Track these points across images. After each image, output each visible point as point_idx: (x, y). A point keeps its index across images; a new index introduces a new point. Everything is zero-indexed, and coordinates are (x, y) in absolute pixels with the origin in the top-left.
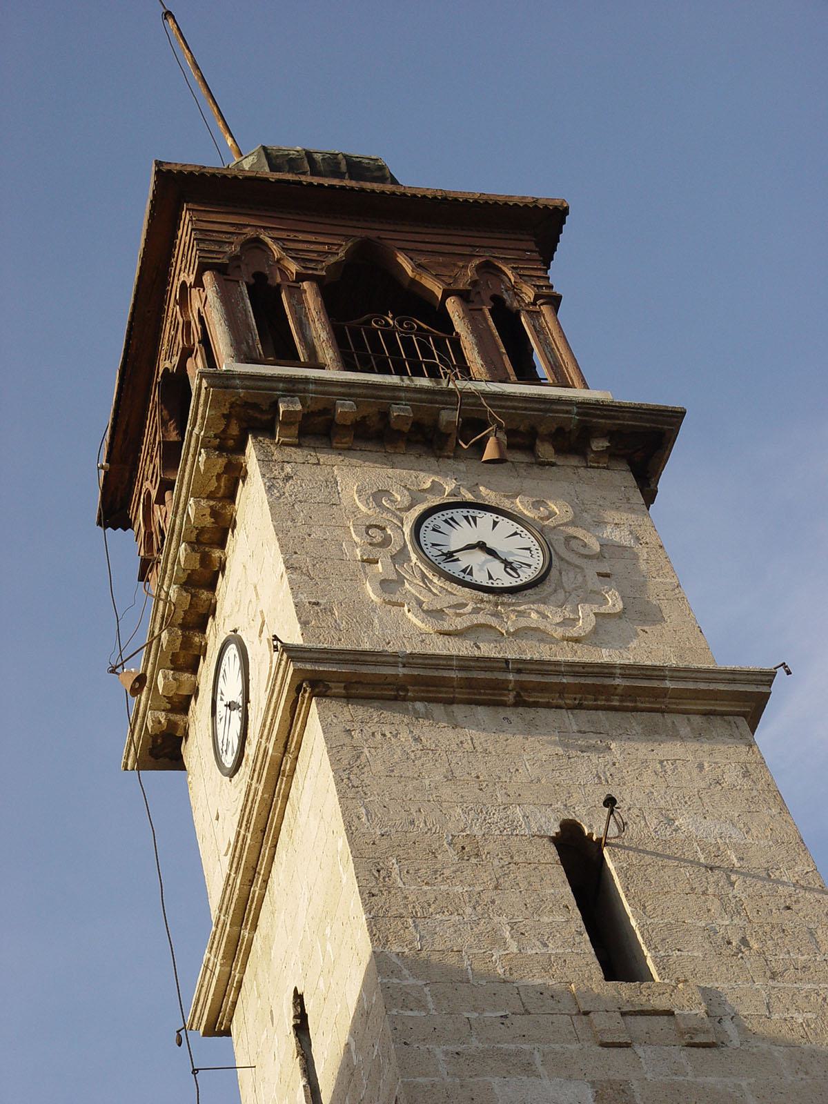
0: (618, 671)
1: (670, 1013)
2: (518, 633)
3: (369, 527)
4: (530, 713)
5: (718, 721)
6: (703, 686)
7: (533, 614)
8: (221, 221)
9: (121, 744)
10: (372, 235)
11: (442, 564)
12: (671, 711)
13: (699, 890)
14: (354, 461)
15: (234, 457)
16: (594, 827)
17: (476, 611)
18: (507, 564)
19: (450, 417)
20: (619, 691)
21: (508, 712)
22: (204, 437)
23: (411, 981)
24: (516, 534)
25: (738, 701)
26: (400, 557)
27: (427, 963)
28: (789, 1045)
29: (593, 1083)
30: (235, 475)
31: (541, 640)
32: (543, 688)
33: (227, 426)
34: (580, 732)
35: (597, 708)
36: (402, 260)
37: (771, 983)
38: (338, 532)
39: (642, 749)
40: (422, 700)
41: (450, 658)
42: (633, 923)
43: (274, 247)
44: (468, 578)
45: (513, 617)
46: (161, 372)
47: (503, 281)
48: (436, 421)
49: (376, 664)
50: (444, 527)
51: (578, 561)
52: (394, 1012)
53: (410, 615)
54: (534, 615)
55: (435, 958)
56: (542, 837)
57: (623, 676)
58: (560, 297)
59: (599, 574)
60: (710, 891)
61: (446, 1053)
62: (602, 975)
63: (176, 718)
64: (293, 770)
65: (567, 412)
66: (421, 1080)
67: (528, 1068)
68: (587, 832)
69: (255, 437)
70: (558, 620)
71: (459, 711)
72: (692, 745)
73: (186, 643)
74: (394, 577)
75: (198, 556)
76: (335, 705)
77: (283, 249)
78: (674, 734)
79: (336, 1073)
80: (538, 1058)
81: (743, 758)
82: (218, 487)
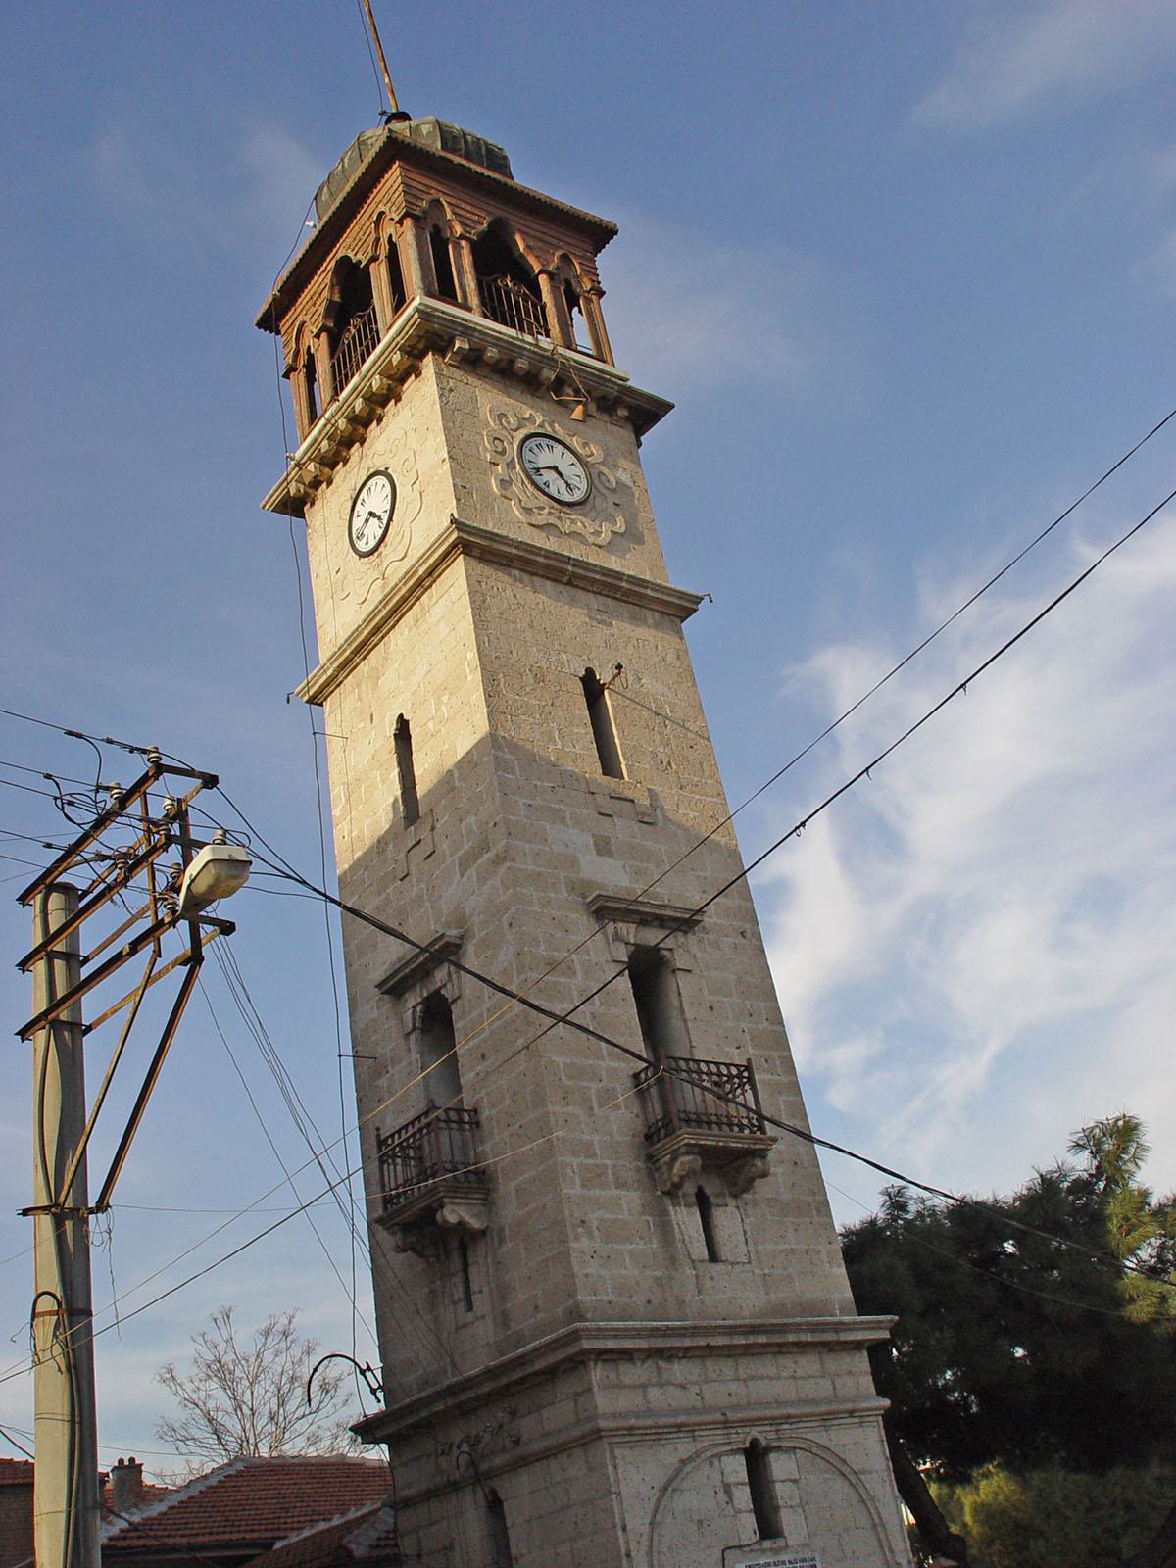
0: (626, 578)
1: (632, 801)
2: (573, 535)
3: (495, 439)
4: (573, 591)
5: (667, 618)
6: (666, 598)
7: (580, 523)
8: (420, 180)
9: (273, 494)
10: (504, 214)
11: (532, 474)
12: (646, 607)
13: (651, 727)
14: (488, 387)
15: (417, 362)
16: (603, 676)
17: (550, 514)
18: (568, 485)
19: (549, 375)
20: (623, 590)
21: (562, 588)
22: (402, 344)
23: (508, 756)
24: (573, 464)
25: (678, 608)
26: (510, 465)
27: (517, 746)
28: (686, 830)
29: (593, 835)
30: (414, 371)
31: (582, 542)
32: (585, 578)
33: (418, 342)
34: (598, 610)
35: (607, 596)
36: (518, 238)
37: (681, 792)
38: (478, 437)
39: (628, 628)
40: (519, 570)
41: (540, 549)
42: (617, 741)
43: (448, 210)
44: (546, 490)
45: (568, 522)
46: (338, 257)
47: (572, 270)
48: (539, 372)
49: (501, 543)
50: (536, 449)
51: (604, 491)
52: (499, 773)
53: (514, 508)
54: (579, 524)
55: (521, 743)
56: (576, 676)
57: (627, 581)
58: (604, 293)
59: (615, 504)
60: (656, 729)
61: (525, 804)
62: (601, 772)
63: (310, 491)
64: (430, 586)
65: (612, 388)
66: (511, 817)
67: (563, 820)
68: (598, 678)
69: (433, 355)
70: (592, 531)
71: (538, 581)
72: (653, 632)
73: (337, 453)
74: (508, 479)
75: (368, 409)
76: (473, 562)
77: (454, 213)
78: (644, 622)
79: (436, 781)
80: (568, 814)
81: (678, 647)
82: (396, 374)
